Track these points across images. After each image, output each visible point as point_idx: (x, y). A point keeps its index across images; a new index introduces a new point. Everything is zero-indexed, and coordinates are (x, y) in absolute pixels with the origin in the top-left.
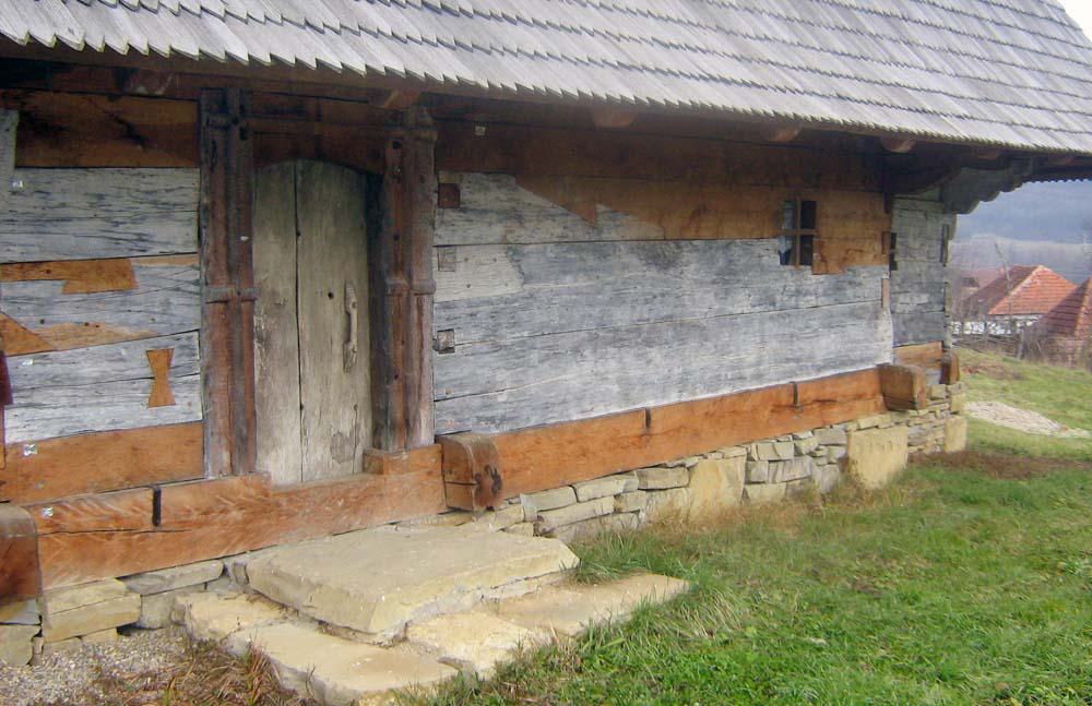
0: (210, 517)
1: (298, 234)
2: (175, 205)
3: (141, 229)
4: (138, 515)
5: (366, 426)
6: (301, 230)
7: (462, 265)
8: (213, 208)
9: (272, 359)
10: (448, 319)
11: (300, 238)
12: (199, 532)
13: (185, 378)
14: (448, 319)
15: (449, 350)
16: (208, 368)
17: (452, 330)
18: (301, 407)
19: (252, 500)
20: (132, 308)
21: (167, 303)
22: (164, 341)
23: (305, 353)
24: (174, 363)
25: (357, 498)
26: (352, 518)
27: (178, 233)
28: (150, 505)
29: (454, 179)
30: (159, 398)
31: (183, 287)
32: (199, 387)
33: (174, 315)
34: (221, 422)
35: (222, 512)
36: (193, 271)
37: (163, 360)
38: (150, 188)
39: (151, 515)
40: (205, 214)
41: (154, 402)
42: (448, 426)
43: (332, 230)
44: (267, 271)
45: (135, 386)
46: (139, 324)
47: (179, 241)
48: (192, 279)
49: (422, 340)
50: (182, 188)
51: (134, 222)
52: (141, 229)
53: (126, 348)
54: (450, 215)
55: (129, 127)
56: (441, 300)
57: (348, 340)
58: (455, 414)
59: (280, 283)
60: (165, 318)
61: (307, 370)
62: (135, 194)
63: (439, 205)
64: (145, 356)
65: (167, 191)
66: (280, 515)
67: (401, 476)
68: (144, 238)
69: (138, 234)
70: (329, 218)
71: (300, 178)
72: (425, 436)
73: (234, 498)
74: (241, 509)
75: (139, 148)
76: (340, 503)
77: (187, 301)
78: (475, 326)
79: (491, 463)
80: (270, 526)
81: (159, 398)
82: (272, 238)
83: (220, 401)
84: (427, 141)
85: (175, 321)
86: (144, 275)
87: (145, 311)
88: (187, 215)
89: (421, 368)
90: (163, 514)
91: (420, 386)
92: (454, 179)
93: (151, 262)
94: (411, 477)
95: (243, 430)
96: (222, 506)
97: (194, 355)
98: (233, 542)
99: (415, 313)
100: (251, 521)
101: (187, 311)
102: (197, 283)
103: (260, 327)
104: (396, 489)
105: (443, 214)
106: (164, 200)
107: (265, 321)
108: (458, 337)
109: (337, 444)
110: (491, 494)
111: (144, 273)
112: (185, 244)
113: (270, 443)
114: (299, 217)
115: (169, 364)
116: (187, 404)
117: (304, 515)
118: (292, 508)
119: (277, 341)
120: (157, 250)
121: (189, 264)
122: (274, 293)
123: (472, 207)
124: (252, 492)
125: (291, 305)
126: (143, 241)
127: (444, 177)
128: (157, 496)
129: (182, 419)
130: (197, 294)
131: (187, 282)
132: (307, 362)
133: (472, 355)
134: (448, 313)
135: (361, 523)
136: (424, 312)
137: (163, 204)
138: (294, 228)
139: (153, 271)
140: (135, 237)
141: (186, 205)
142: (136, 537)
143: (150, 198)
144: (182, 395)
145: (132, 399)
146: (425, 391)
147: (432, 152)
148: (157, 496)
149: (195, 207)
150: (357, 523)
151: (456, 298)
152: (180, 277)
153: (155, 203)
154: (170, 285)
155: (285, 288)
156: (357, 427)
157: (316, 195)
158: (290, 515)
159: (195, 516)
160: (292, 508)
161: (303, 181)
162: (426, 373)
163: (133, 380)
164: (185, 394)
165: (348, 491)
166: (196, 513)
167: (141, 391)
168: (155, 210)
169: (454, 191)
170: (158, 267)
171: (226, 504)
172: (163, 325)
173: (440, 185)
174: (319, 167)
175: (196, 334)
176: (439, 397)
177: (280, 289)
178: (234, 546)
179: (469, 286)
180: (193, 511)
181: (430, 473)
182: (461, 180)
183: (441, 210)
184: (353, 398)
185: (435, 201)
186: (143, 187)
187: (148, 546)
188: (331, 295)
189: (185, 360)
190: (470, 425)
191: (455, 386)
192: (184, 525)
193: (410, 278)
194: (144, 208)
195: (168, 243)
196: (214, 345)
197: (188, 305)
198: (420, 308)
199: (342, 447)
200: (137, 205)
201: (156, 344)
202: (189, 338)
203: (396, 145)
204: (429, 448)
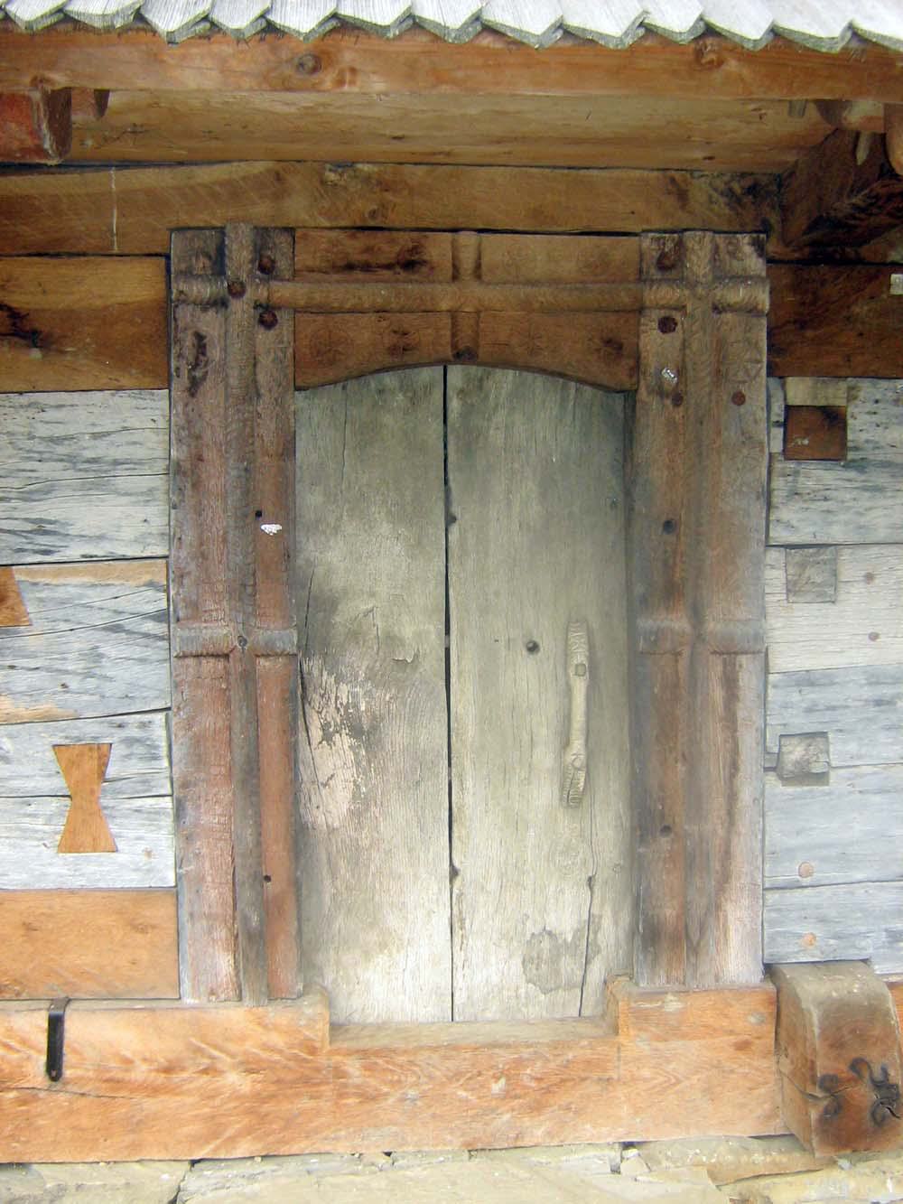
0: (177, 1077)
1: (450, 519)
2: (116, 463)
3: (41, 510)
4: (16, 1056)
5: (616, 923)
6: (456, 510)
7: (858, 589)
8: (194, 467)
9: (383, 770)
10: (809, 710)
11: (454, 529)
12: (151, 1104)
13: (138, 803)
14: (809, 710)
15: (807, 776)
16: (185, 785)
17: (823, 734)
18: (454, 873)
19: (276, 1057)
20: (19, 662)
21: (95, 656)
22: (90, 729)
23: (465, 760)
24: (111, 771)
25: (539, 1080)
26: (527, 1121)
27: (130, 519)
28: (42, 1040)
29: (834, 394)
30: (84, 830)
31: (129, 624)
32: (168, 822)
33: (110, 679)
34: (213, 894)
35: (205, 1071)
36: (150, 593)
37: (90, 765)
38: (59, 431)
39: (44, 1058)
40: (185, 476)
41: (71, 842)
42: (801, 942)
43: (535, 509)
44: (372, 595)
45: (30, 809)
46: (33, 693)
47: (128, 533)
48: (151, 608)
49: (735, 751)
50: (125, 429)
51: (27, 497)
52: (41, 510)
53: (10, 736)
54: (817, 475)
55: (15, 315)
56: (791, 667)
57: (566, 744)
58: (823, 920)
59: (405, 618)
60: (91, 683)
61: (469, 799)
62: (29, 444)
63: (788, 454)
64: (50, 755)
65: (95, 436)
66: (341, 1096)
67: (661, 1045)
68: (49, 527)
69: (33, 521)
70: (530, 487)
71: (454, 404)
72: (736, 961)
73: (232, 1047)
74: (250, 1071)
75: (36, 354)
76: (498, 1087)
77: (138, 652)
78: (889, 728)
79: (874, 1056)
80: (318, 1113)
81: (84, 830)
82: (385, 528)
83: (213, 861)
84: (753, 311)
85: (109, 689)
86: (41, 600)
87: (48, 670)
88: (146, 483)
89: (731, 813)
90: (68, 1057)
91: (727, 854)
92: (834, 394)
93: (57, 574)
94: (688, 1052)
95: (276, 905)
96: (206, 1061)
97: (155, 758)
98: (230, 1132)
99: (718, 694)
100: (273, 1096)
101: (141, 673)
102: (161, 617)
103: (356, 706)
104: (646, 1073)
105: (796, 473)
106: (89, 454)
107: (368, 694)
108: (840, 749)
109: (542, 957)
110: (869, 1124)
111: (43, 595)
112: (140, 540)
113: (373, 937)
114: (452, 484)
115: (102, 775)
116: (143, 850)
117: (402, 1100)
118: (373, 1082)
119: (396, 735)
120: (75, 551)
121: (147, 578)
122: (391, 640)
123: (880, 456)
124: (278, 1040)
125: (433, 664)
126: (46, 533)
127: (800, 390)
128: (55, 1025)
129: (133, 880)
130: (162, 638)
131: (138, 614)
132: (469, 783)
133: (881, 791)
134: (812, 695)
135: (549, 1134)
136: (741, 693)
137: (89, 461)
138: (441, 505)
139: (61, 593)
140: (29, 527)
141: (140, 462)
142: (12, 1095)
143: (61, 450)
144: (132, 834)
145: (26, 834)
146: (742, 866)
147: (764, 335)
148: (55, 1025)
149: (161, 466)
150: (539, 1132)
151: (840, 661)
152: (122, 604)
153: (71, 460)
154: (100, 619)
155: (418, 630)
156: (592, 923)
157: (496, 437)
158: (368, 1097)
159: (141, 1073)
160: (373, 1082)
161: (467, 413)
162: (743, 826)
163: (28, 798)
164: (141, 832)
165: (519, 1063)
166: (145, 1067)
167: (50, 817)
168: (70, 474)
169: (833, 419)
170: (71, 585)
171: (212, 1058)
172: (86, 698)
173: (788, 408)
174: (505, 380)
175: (161, 717)
176: (781, 880)
177: (407, 631)
178: (232, 1140)
179: (874, 637)
180: (138, 1062)
181: (743, 1046)
182: (851, 398)
183: (792, 465)
184: (584, 862)
185: (777, 446)
186: (43, 431)
187: (40, 1115)
188: (533, 648)
189: (135, 767)
190: (867, 947)
191: (823, 860)
192: (114, 1084)
193: (697, 616)
194: (45, 470)
195: (101, 538)
196: (197, 741)
197: (142, 661)
198: (730, 683)
199: (555, 960)
200: (36, 465)
201: (76, 733)
202: (143, 725)
203: (666, 325)
204: (741, 991)
